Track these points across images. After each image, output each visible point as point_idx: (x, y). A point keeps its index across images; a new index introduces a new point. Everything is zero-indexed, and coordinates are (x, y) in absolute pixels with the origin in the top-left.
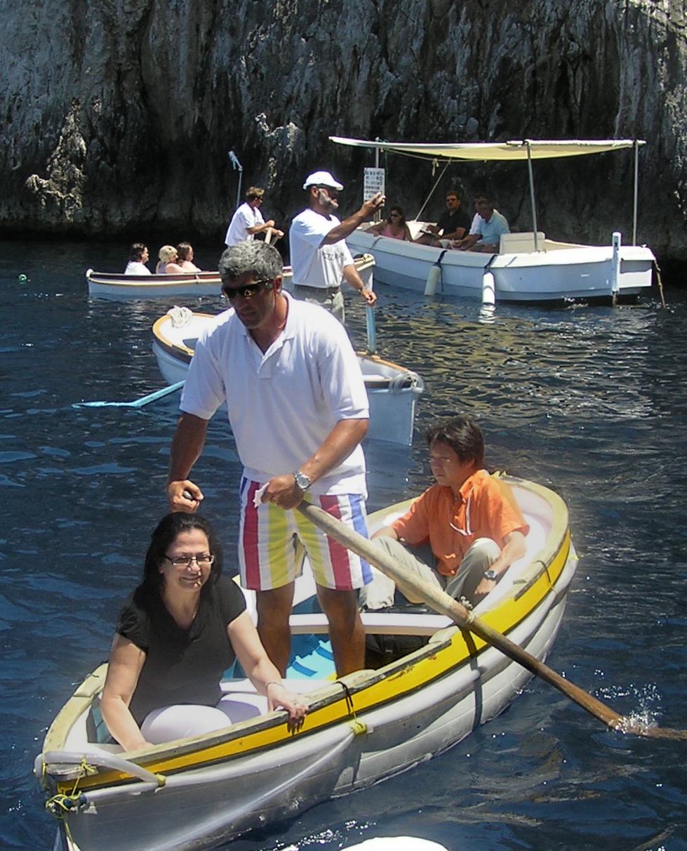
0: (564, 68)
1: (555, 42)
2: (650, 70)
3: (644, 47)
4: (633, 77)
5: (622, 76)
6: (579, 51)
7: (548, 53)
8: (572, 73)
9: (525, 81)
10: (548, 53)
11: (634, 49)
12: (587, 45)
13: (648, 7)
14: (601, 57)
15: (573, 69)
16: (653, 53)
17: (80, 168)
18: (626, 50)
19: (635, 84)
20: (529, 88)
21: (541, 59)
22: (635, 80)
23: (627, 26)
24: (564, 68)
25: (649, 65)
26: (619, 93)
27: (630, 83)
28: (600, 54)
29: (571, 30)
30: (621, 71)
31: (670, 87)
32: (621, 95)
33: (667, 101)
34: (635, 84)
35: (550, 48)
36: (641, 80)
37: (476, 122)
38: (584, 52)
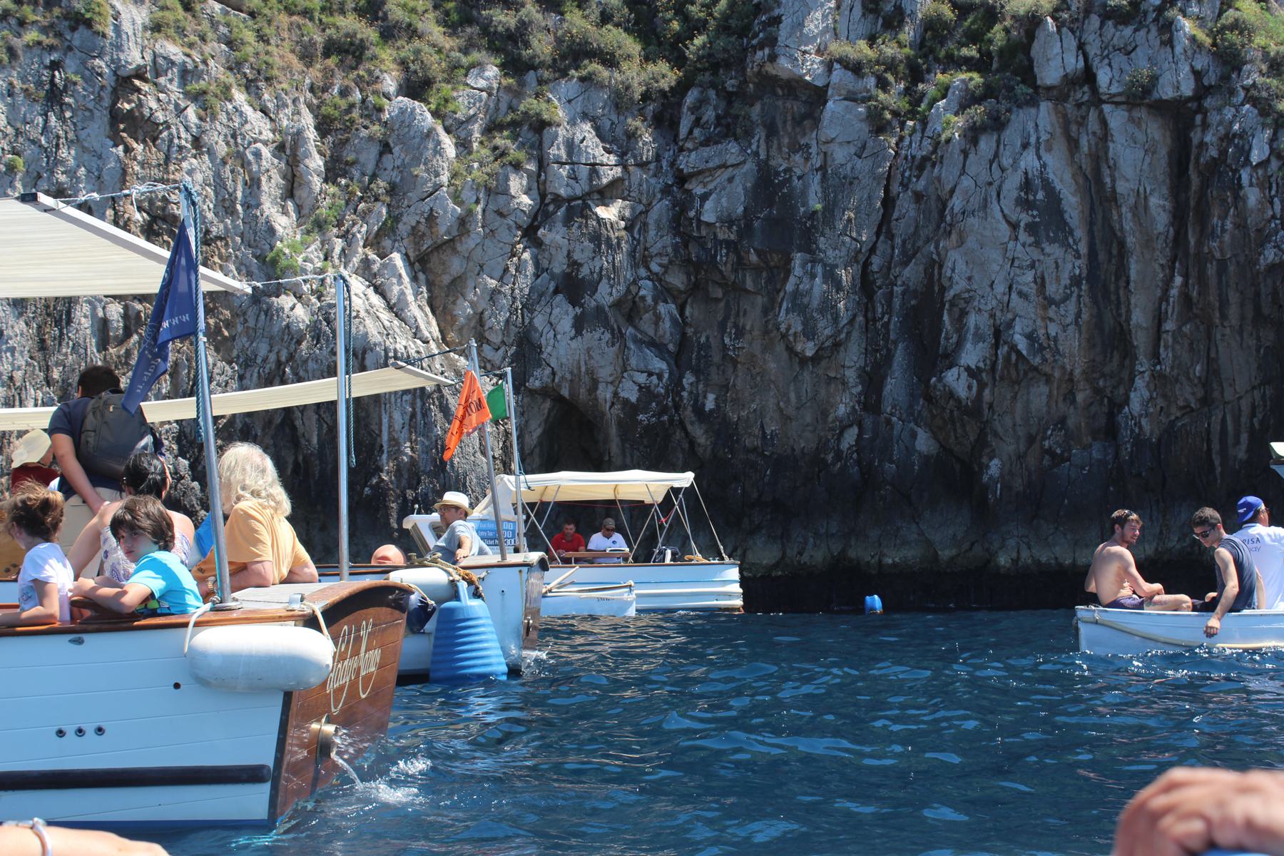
2: (419, 416)
5: (385, 420)
16: (422, 400)
25: (418, 410)
26: (380, 435)
27: (397, 427)
32: (385, 437)
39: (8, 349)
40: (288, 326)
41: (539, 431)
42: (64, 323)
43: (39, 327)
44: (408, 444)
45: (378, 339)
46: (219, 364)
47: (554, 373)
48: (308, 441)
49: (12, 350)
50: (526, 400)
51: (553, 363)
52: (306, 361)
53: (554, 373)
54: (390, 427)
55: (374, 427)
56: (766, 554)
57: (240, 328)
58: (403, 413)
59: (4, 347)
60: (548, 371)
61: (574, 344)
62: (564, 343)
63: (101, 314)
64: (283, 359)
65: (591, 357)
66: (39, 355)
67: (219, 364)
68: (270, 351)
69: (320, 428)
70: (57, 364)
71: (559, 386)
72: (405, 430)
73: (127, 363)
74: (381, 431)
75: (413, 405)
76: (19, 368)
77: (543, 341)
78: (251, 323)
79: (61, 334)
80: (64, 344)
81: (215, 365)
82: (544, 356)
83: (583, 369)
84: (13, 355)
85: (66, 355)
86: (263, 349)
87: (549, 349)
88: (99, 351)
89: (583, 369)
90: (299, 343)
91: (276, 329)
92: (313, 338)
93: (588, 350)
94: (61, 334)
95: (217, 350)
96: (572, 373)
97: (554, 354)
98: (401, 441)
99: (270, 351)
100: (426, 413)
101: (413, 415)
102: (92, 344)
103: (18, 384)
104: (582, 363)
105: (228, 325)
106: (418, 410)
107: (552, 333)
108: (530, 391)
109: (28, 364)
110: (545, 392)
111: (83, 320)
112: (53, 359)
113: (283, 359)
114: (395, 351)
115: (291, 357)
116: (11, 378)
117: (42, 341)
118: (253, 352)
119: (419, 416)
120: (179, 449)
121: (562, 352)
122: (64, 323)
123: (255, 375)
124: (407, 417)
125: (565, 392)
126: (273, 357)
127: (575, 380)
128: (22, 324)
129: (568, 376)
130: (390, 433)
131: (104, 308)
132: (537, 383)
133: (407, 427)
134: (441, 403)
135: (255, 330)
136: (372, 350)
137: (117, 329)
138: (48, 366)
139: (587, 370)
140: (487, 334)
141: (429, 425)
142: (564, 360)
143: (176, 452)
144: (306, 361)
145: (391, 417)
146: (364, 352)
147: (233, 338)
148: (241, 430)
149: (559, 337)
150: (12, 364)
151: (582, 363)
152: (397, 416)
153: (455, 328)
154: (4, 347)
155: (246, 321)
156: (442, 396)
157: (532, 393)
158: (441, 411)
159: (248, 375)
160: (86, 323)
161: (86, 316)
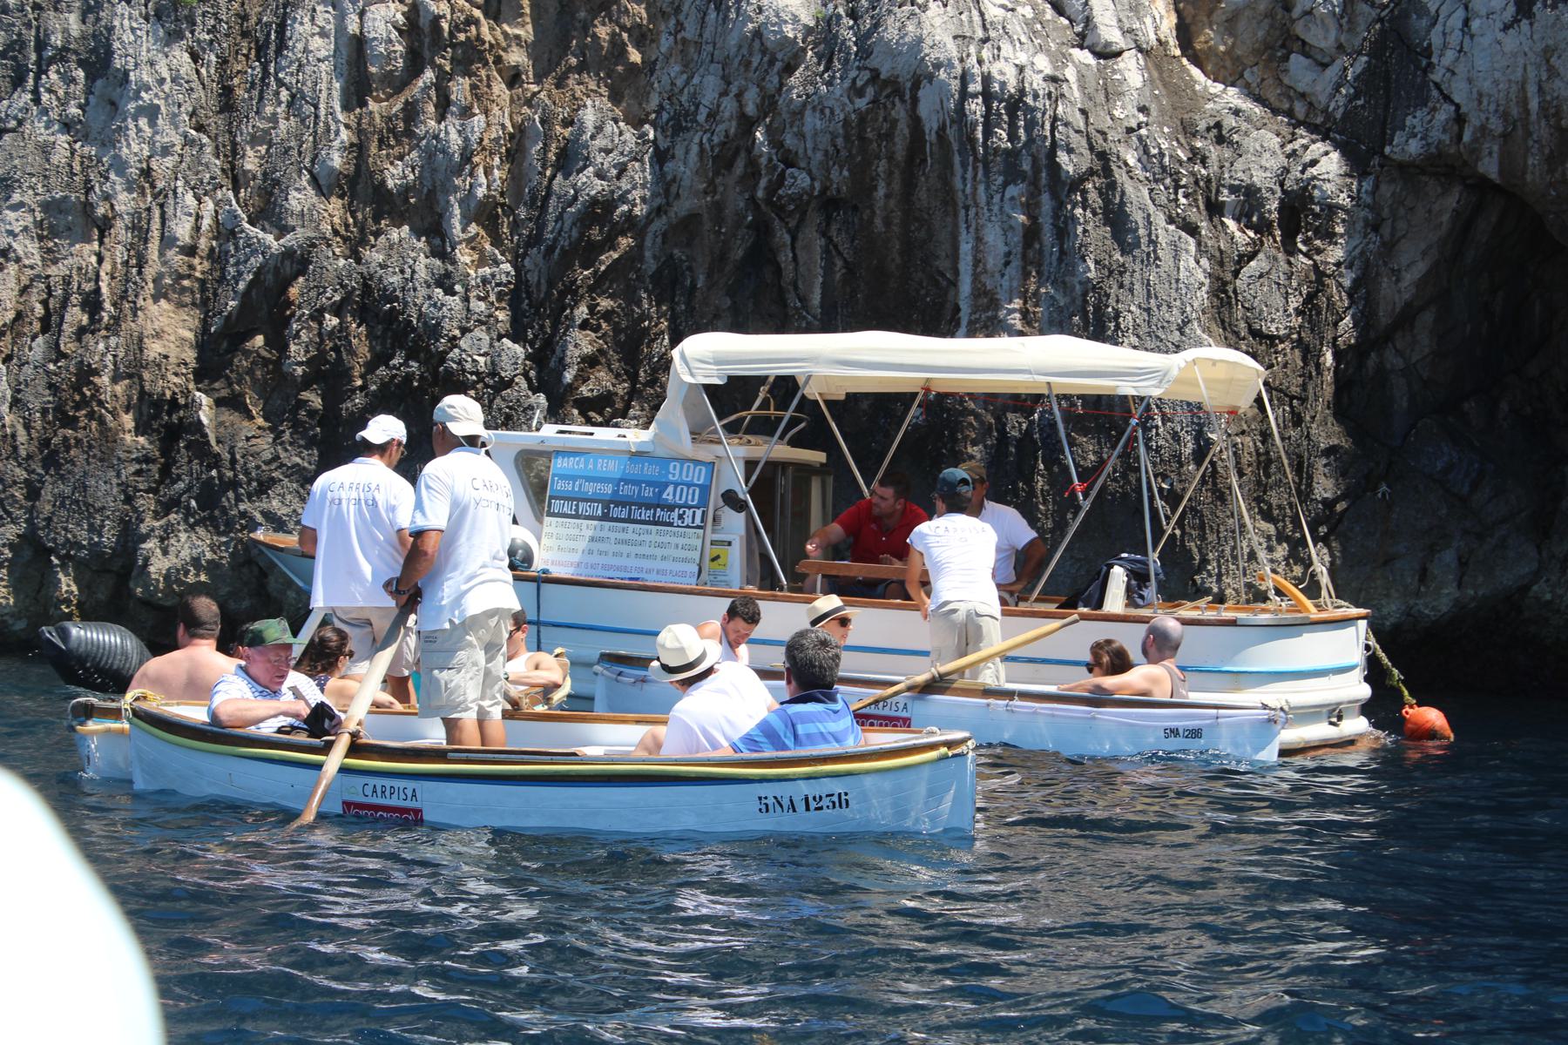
0: (762, 230)
1: (729, 166)
2: (1048, 236)
3: (1035, 183)
4: (1003, 249)
5: (966, 248)
6: (812, 187)
7: (706, 193)
8: (787, 238)
9: (648, 254)
10: (706, 193)
11: (1005, 185)
12: (840, 176)
13: (1041, 93)
14: (892, 203)
15: (789, 231)
16: (1055, 195)
17: (595, 36)
18: (981, 188)
19: (1007, 264)
20: (659, 271)
21: (683, 207)
22: (1008, 254)
23: (988, 133)
24: (762, 230)
25: (1046, 222)
26: (954, 284)
27: (993, 261)
28: (887, 196)
29: (789, 140)
30: (963, 236)
31: (599, 285)
32: (965, 287)
33: (1112, 301)
34: (1007, 264)
35: (711, 183)
36: (1024, 256)
37: (518, 349)
38: (824, 190)
39: (141, 111)
40: (758, 34)
41: (1421, 267)
42: (271, 52)
43: (223, 62)
44: (1017, 303)
45: (952, 49)
46: (610, 127)
47: (1460, 119)
48: (803, 300)
49: (152, 112)
50: (1386, 190)
51: (1459, 92)
52: (798, 114)
53: (1460, 119)
54: (977, 262)
55: (943, 264)
56: (1393, 609)
57: (665, 43)
58: (1007, 229)
59: (131, 106)
60: (1444, 113)
61: (1511, 41)
62: (1486, 41)
63: (353, 26)
64: (750, 109)
65: (1553, 73)
66: (216, 122)
67: (610, 127)
68: (724, 94)
69: (828, 270)
70: (254, 141)
71: (1474, 151)
72: (1013, 270)
73: (409, 133)
74: (956, 272)
75: (1031, 208)
76: (166, 151)
77: (1436, 38)
78: (690, 32)
79: (266, 73)
80: (269, 95)
81: (599, 129)
82: (1436, 76)
83: (1534, 105)
84: (152, 123)
85: (274, 119)
86: (710, 86)
87: (1450, 55)
88: (346, 107)
89: (1534, 105)
90: (789, 69)
91: (733, 41)
92: (819, 56)
93: (1548, 53)
94: (266, 73)
95: (615, 98)
96: (1505, 116)
97: (1461, 69)
98: (1001, 296)
99: (724, 94)
100: (1064, 228)
101: (1031, 234)
102: (331, 92)
103: (160, 185)
104: (1532, 89)
105: (642, 37)
106: (1046, 222)
107: (1460, 13)
108: (1402, 166)
109: (188, 142)
110: (1444, 167)
111: (316, 42)
112: (247, 129)
113: (750, 109)
114: (987, 79)
115: (769, 103)
116: (147, 173)
117: (227, 91)
118: (694, 96)
119: (1048, 236)
120: (515, 320)
121: (1481, 63)
122: (271, 52)
123: (695, 149)
124: (1016, 238)
125: (1489, 167)
126: (729, 106)
127: (1514, 131)
128: (180, 57)
129: (1496, 125)
130: (976, 277)
131: (362, 14)
132: (1414, 147)
133: (1016, 263)
134: (1107, 202)
135: (698, 45)
136: (931, 78)
137: (389, 58)
138: (234, 144)
139: (1543, 107)
140: (1299, 29)
141: (1069, 256)
142: (1486, 86)
143: (503, 327)
144: (798, 114)
145: (979, 239)
146: (916, 86)
147: (649, 66)
148: (657, 277)
149: (1475, 24)
150: (151, 143)
151: (1532, 89)
152: (993, 236)
153: (1218, 16)
154: (131, 106)
155: (680, 26)
156: (1112, 185)
157: (1406, 171)
158: (1107, 221)
159: (679, 151)
160: (322, 47)
161: (323, 34)
